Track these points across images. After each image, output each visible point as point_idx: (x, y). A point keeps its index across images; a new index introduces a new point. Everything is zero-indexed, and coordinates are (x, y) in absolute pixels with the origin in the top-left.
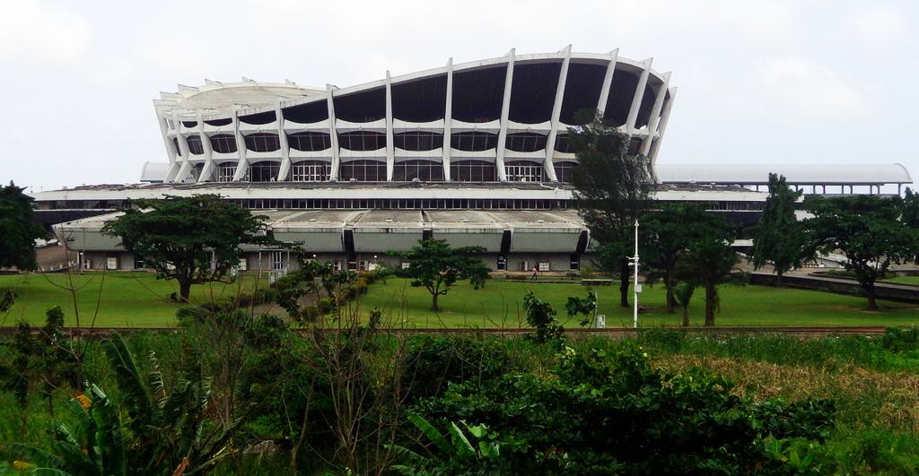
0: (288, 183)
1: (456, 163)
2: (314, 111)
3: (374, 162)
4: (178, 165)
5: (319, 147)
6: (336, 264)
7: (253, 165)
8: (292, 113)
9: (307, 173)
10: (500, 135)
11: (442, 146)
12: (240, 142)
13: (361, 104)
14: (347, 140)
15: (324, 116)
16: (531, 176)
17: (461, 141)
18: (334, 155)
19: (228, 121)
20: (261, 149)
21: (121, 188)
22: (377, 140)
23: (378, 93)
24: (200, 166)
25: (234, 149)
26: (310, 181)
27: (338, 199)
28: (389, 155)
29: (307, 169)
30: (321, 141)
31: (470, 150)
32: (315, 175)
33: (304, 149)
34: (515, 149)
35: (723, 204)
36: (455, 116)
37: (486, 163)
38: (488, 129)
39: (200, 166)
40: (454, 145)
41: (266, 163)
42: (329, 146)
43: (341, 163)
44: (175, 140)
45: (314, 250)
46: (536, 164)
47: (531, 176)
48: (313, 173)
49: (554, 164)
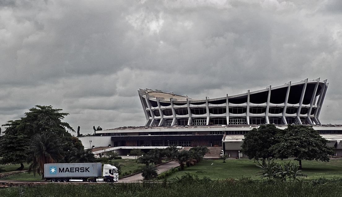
0: (162, 125)
1: (251, 118)
2: (243, 99)
3: (222, 118)
4: (150, 121)
5: (221, 113)
6: (228, 154)
7: (178, 119)
8: (232, 100)
9: (198, 122)
10: (285, 107)
11: (226, 112)
12: (173, 112)
13: (259, 97)
14: (253, 110)
15: (246, 101)
16: (242, 122)
17: (272, 110)
18: (248, 115)
19: (205, 103)
20: (197, 113)
21: (134, 128)
22: (263, 110)
23: (266, 93)
24: (159, 120)
25: (171, 114)
26: (235, 124)
27: (240, 131)
28: (227, 115)
29: (198, 121)
30: (244, 110)
31: (256, 113)
32: (233, 122)
33: (214, 114)
34: (254, 113)
35: (211, 132)
36: (271, 102)
37: (261, 118)
38: (222, 106)
39: (159, 120)
40: (250, 112)
41: (183, 119)
42: (206, 113)
43: (210, 119)
44: (149, 111)
45: (238, 149)
46: (243, 118)
47: (237, 122)
48: (200, 122)
49: (269, 118)
